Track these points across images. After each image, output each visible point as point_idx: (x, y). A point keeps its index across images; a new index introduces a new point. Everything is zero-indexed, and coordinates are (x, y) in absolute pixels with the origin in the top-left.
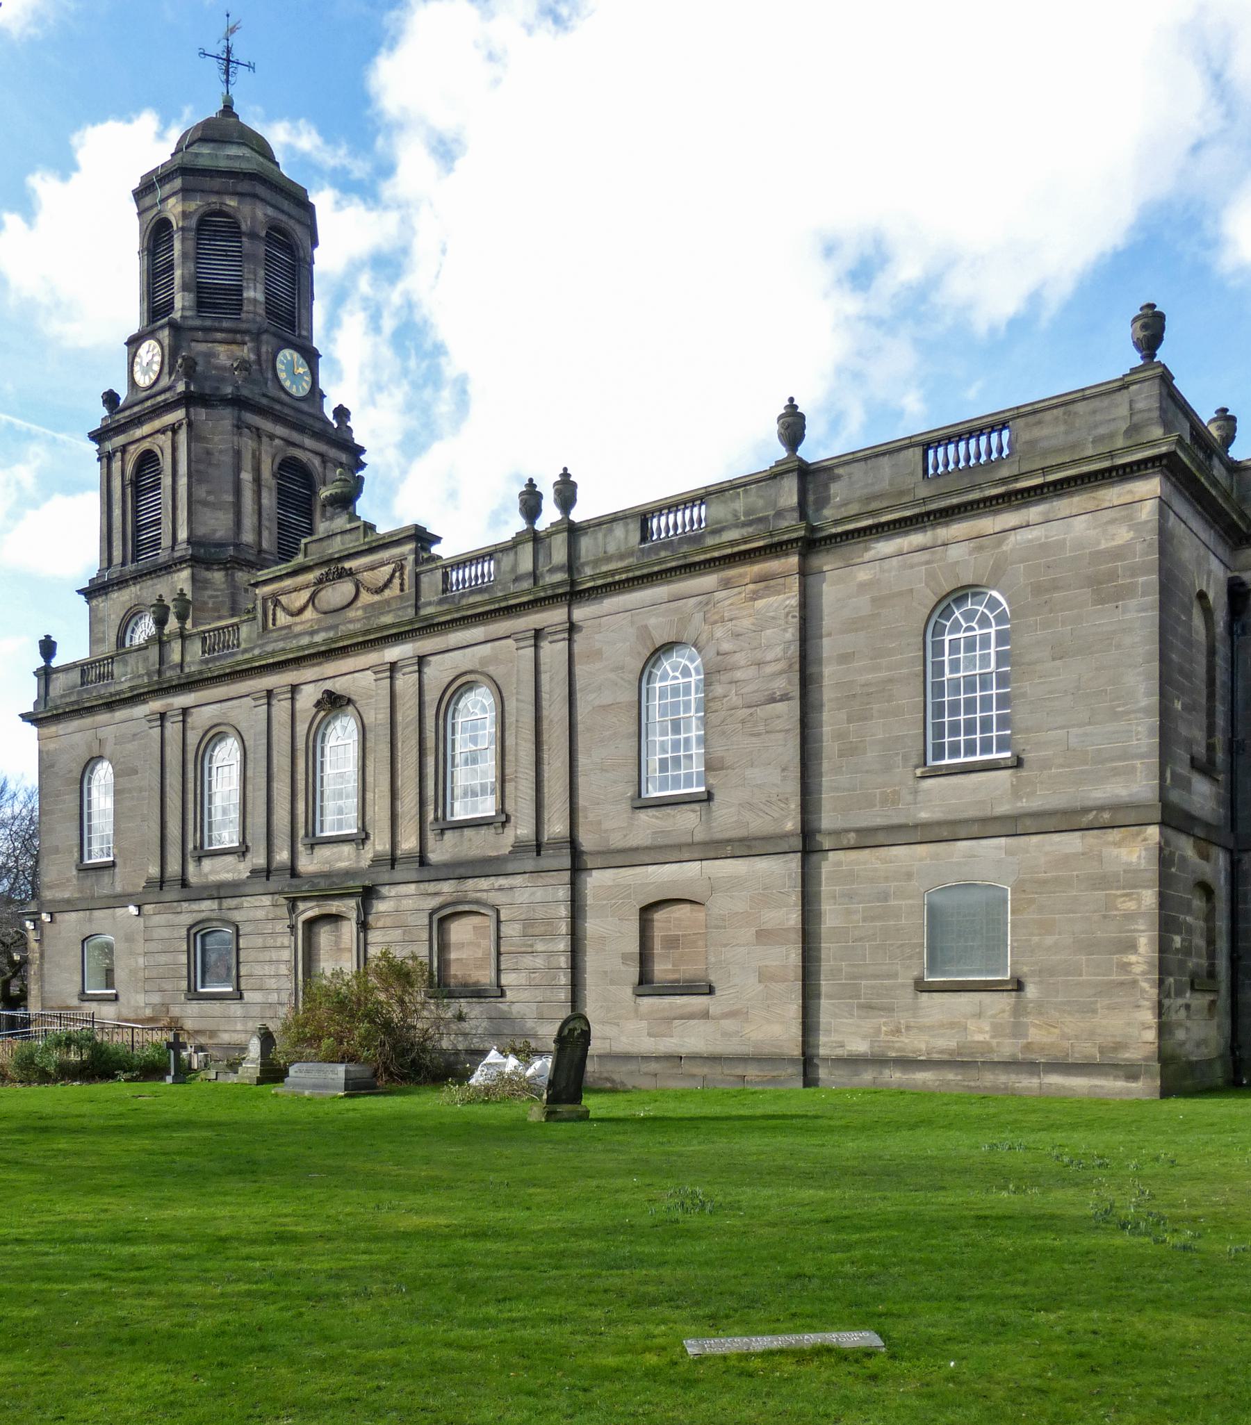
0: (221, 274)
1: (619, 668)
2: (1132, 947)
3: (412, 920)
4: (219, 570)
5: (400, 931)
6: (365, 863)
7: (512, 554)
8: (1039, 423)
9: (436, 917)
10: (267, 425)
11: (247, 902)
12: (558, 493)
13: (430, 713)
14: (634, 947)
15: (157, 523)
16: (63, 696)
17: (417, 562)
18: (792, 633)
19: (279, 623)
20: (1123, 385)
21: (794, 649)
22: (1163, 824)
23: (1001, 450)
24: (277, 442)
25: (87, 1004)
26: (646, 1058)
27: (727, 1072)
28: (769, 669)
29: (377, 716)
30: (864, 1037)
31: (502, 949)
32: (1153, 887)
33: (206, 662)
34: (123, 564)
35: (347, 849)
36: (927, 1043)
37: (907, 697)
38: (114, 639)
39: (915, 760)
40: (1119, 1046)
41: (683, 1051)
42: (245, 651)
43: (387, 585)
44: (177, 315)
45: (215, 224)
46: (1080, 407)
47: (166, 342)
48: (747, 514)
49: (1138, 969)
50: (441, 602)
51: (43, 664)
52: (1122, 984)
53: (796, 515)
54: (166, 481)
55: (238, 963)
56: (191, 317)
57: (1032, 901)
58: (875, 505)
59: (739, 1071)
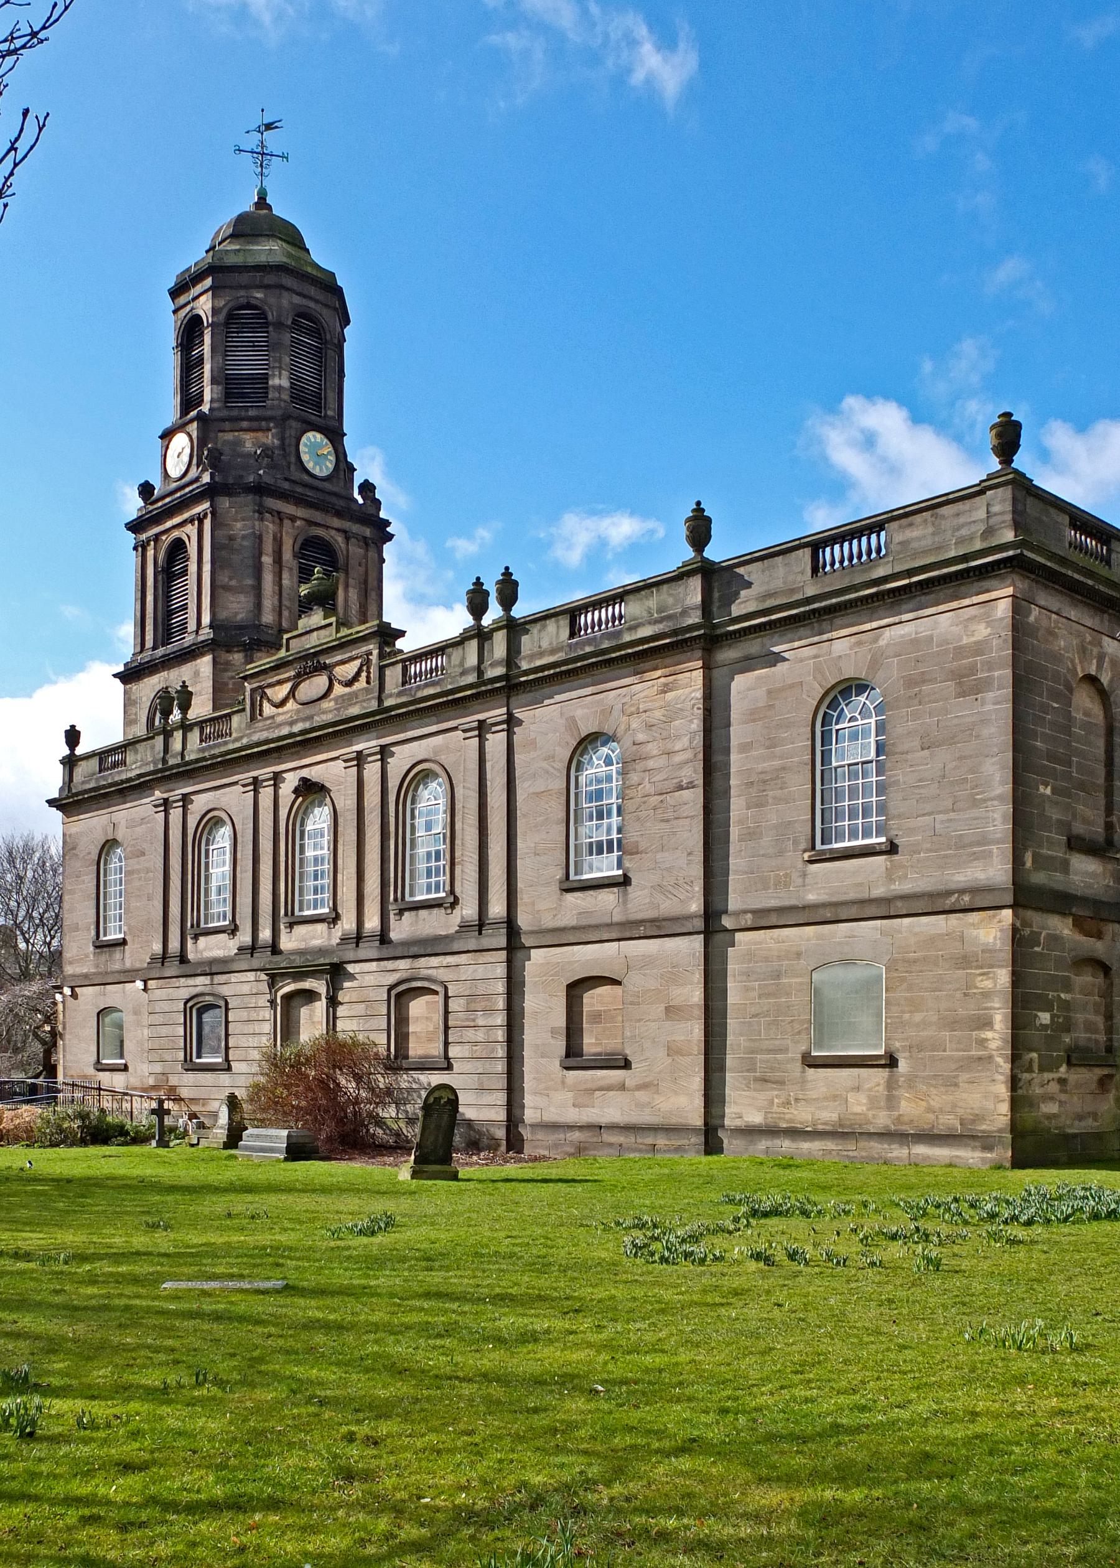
0: (246, 364)
1: (550, 758)
2: (988, 1024)
3: (373, 995)
4: (238, 652)
5: (363, 1005)
6: (335, 941)
7: (460, 648)
8: (911, 525)
9: (393, 993)
10: (289, 509)
11: (234, 978)
12: (500, 592)
13: (392, 798)
14: (561, 1022)
15: (184, 607)
16: (83, 783)
17: (381, 656)
18: (697, 725)
19: (265, 715)
20: (980, 490)
21: (699, 740)
22: (1015, 906)
23: (879, 550)
24: (298, 523)
25: (101, 1073)
26: (571, 1127)
27: (639, 1140)
28: (678, 758)
29: (346, 801)
30: (759, 1109)
31: (450, 1023)
32: (1007, 966)
33: (203, 750)
34: (154, 648)
35: (321, 928)
36: (813, 1114)
37: (799, 784)
38: (144, 719)
39: (803, 845)
40: (978, 1118)
41: (603, 1120)
42: (236, 740)
43: (356, 678)
44: (205, 408)
45: (242, 316)
46: (945, 510)
47: (195, 435)
48: (659, 611)
49: (993, 1045)
50: (400, 694)
51: (68, 752)
52: (980, 1059)
53: (699, 613)
54: (193, 568)
55: (227, 1035)
56: (219, 409)
57: (902, 980)
58: (769, 603)
59: (649, 1140)
